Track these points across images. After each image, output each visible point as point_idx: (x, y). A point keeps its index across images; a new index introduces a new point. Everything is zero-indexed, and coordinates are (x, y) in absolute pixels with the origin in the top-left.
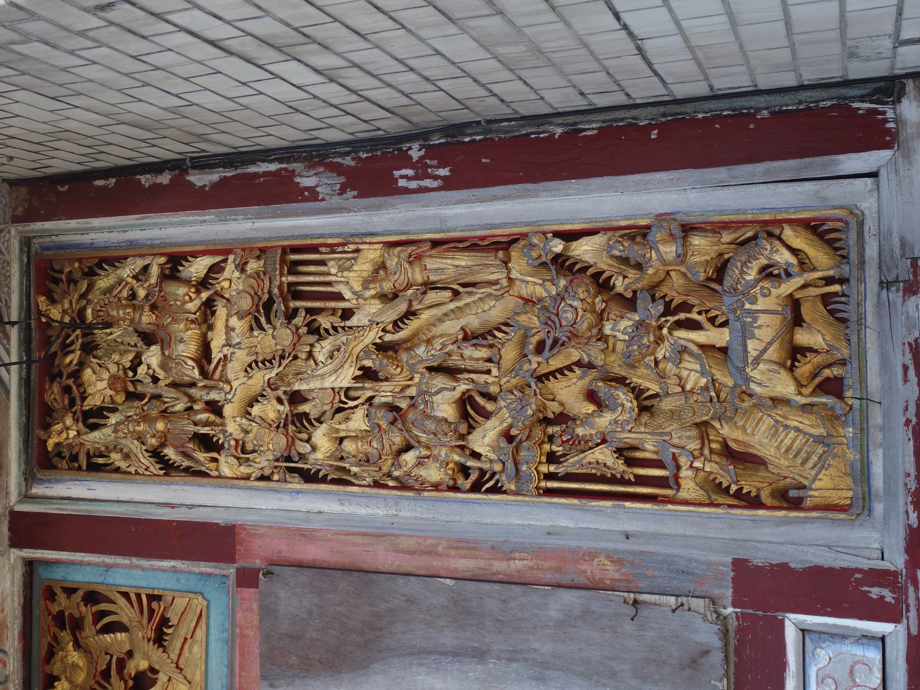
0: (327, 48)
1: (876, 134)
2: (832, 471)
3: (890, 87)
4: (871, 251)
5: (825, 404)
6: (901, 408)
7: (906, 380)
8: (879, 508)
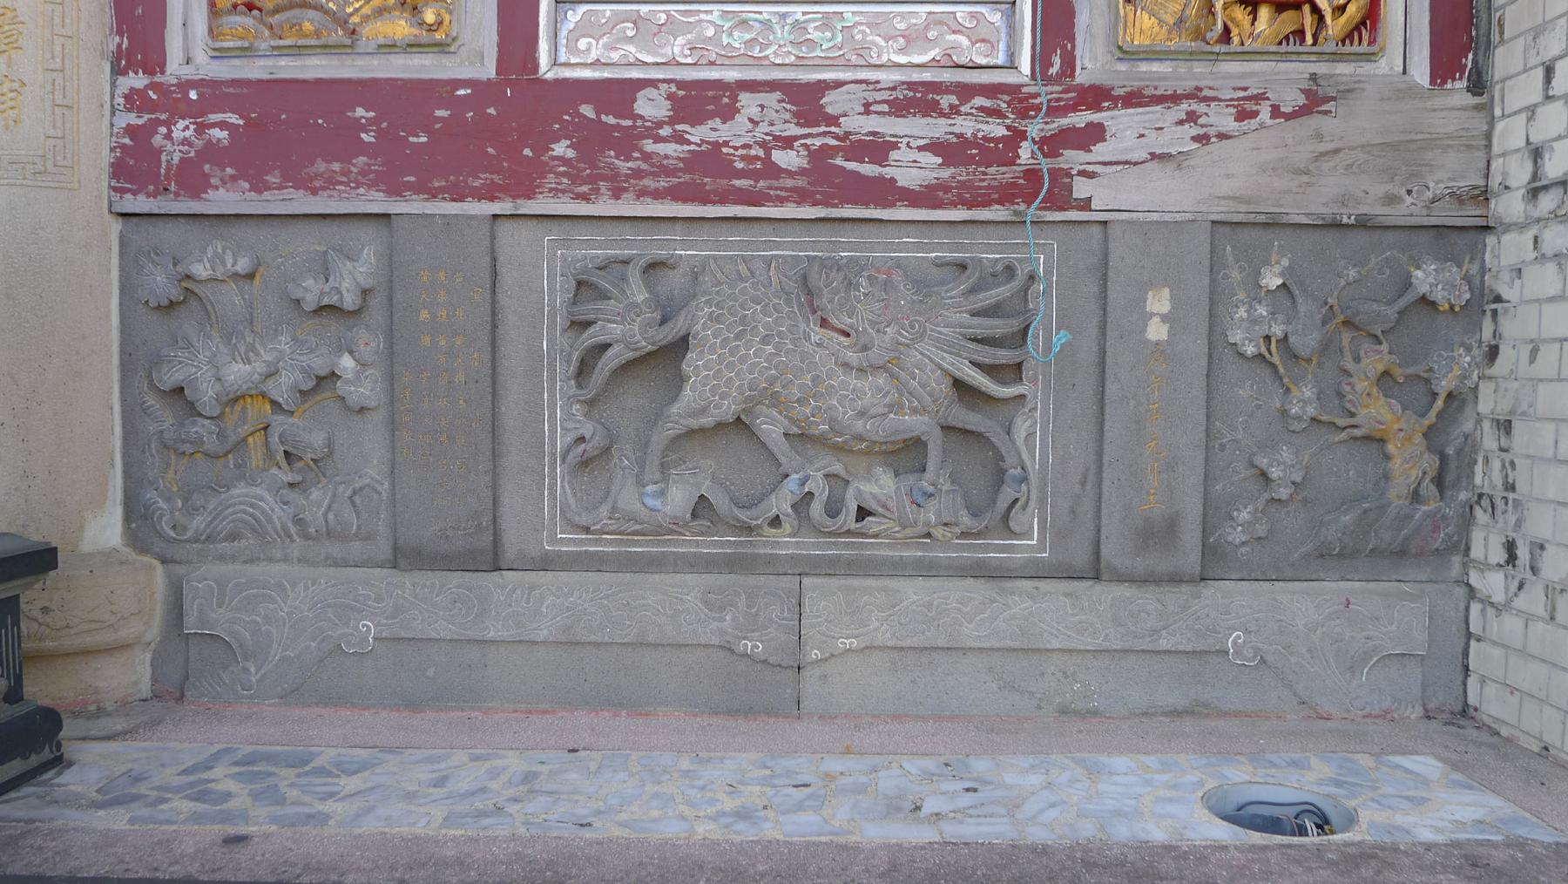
0: (1145, 714)
1: (1443, 69)
2: (1157, 29)
3: (1478, 85)
4: (1343, 69)
5: (1215, 24)
6: (1211, 84)
7: (1235, 89)
8: (1122, 67)
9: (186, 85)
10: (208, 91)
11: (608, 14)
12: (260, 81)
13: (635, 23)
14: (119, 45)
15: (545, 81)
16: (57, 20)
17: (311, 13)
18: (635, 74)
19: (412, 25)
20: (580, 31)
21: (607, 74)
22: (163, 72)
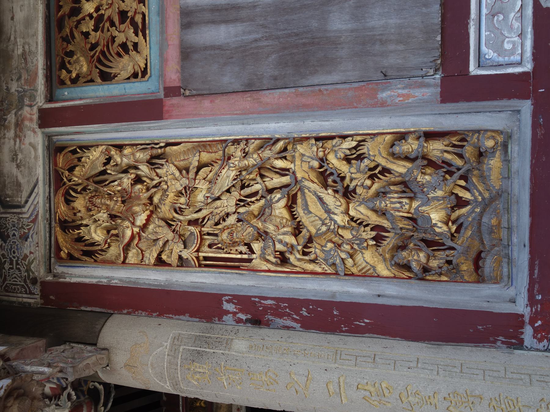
9: (532, 301)
10: (537, 286)
11: (488, 33)
12: (531, 252)
13: (493, 16)
14: (503, 343)
15: (534, 69)
16: (495, 374)
17: (485, 220)
18: (529, 11)
19: (494, 157)
20: (499, 49)
21: (529, 30)
22: (522, 316)
